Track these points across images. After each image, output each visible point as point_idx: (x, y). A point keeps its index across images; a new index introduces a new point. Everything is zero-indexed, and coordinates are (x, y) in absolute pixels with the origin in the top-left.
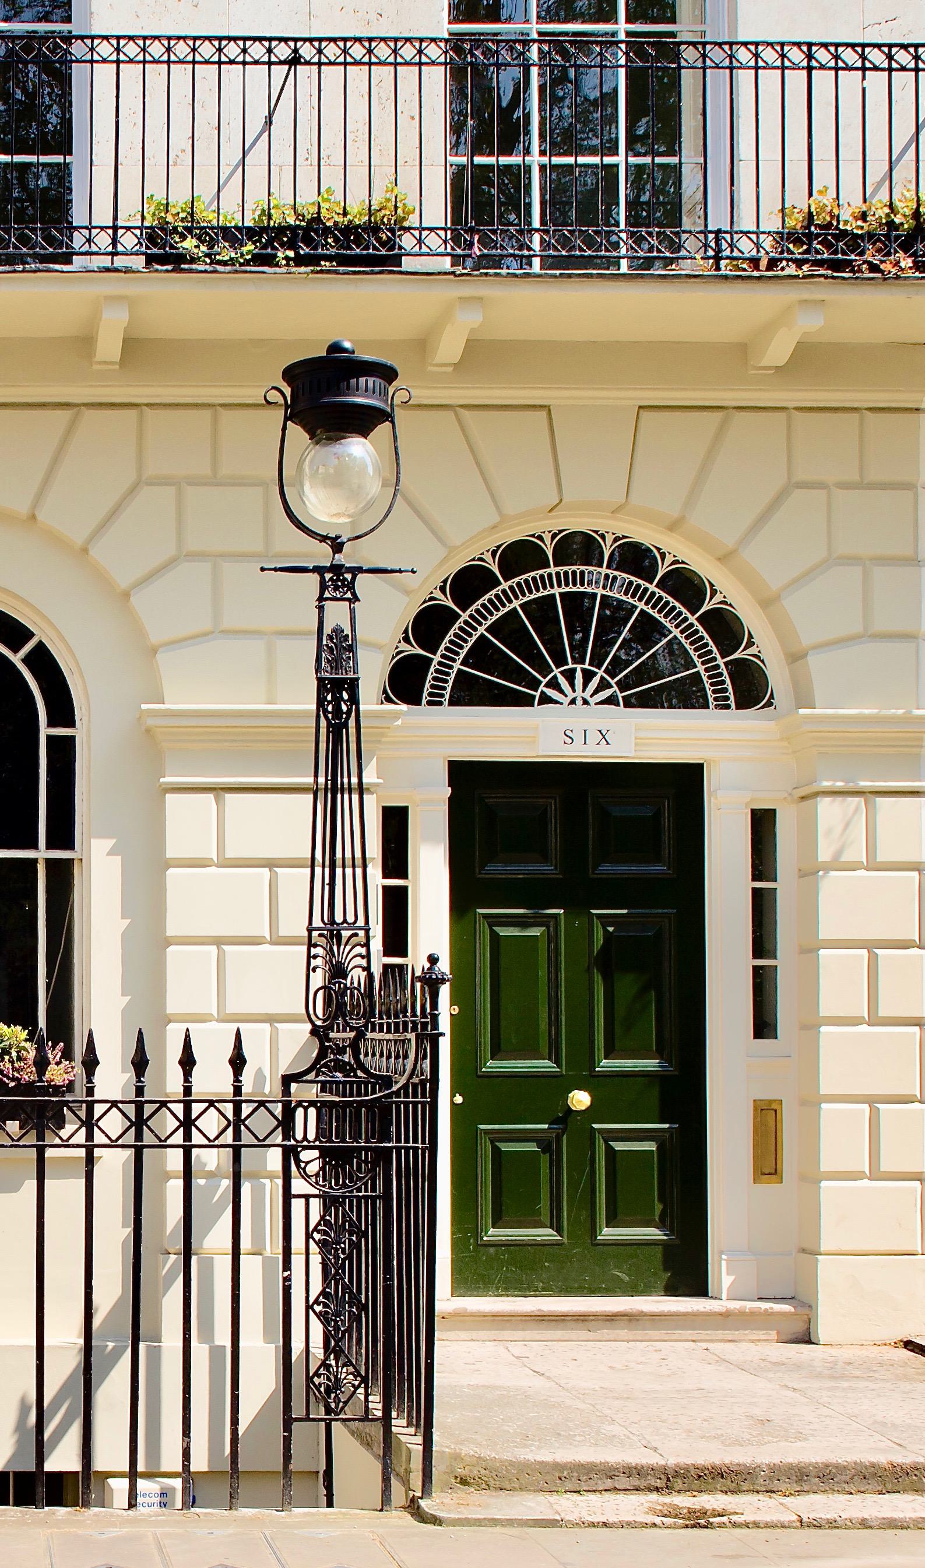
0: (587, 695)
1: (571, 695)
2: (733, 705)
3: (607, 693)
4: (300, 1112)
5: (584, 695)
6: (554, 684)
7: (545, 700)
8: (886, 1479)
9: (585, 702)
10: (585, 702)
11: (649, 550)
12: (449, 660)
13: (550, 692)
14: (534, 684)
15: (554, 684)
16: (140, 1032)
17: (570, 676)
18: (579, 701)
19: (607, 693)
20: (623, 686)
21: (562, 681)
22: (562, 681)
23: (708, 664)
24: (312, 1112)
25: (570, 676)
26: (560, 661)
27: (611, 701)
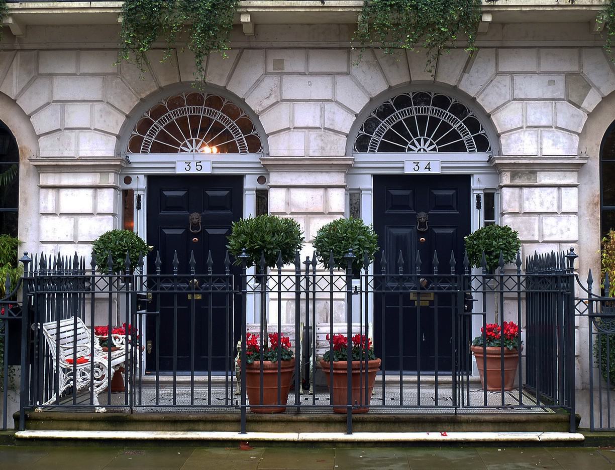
0: (425, 148)
1: (191, 149)
2: (248, 152)
3: (433, 147)
4: (594, 302)
5: (196, 149)
6: (185, 145)
7: (410, 149)
8: (334, 276)
9: (425, 150)
10: (425, 150)
11: (425, 93)
12: (149, 138)
13: (411, 147)
14: (406, 144)
15: (185, 145)
16: (42, 252)
17: (419, 141)
18: (422, 150)
19: (433, 147)
20: (438, 144)
21: (188, 144)
22: (188, 144)
23: (467, 137)
24: (599, 302)
25: (419, 141)
26: (415, 135)
27: (434, 149)
